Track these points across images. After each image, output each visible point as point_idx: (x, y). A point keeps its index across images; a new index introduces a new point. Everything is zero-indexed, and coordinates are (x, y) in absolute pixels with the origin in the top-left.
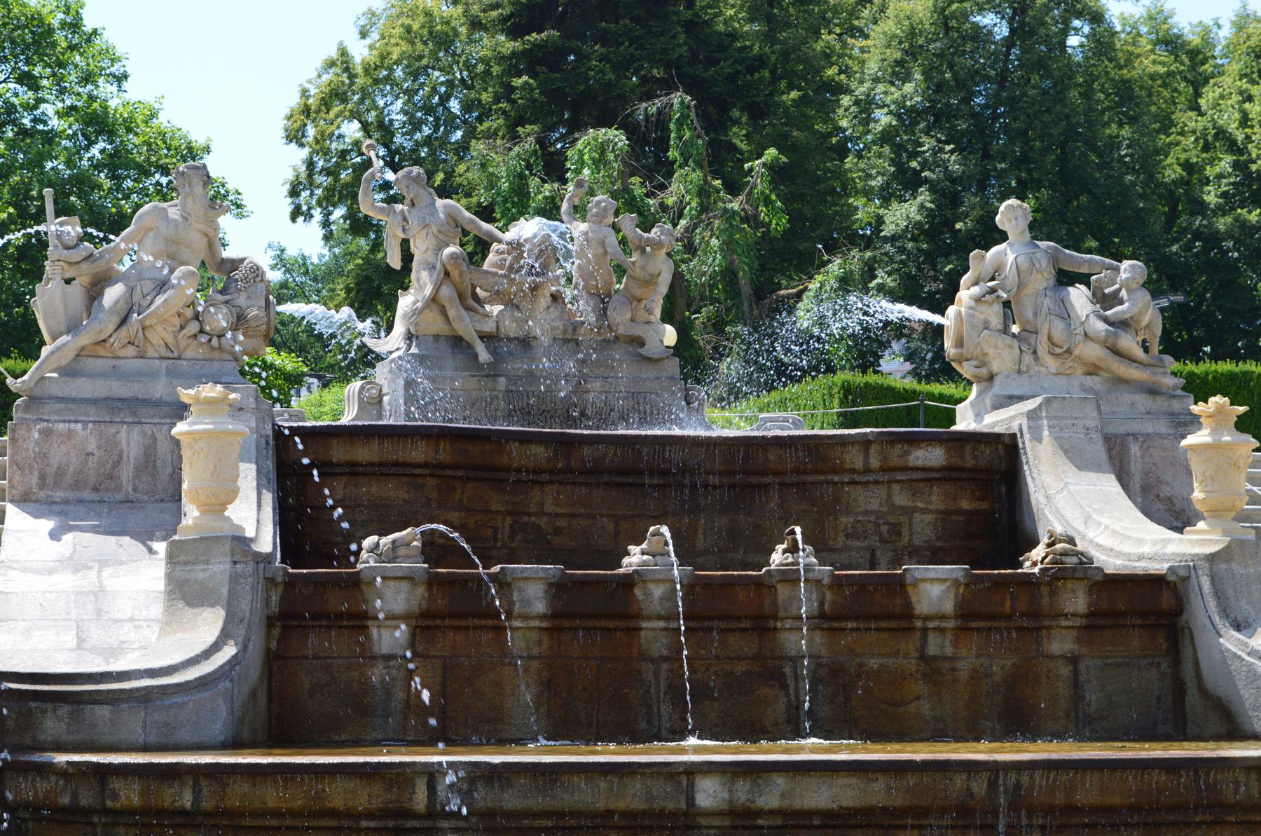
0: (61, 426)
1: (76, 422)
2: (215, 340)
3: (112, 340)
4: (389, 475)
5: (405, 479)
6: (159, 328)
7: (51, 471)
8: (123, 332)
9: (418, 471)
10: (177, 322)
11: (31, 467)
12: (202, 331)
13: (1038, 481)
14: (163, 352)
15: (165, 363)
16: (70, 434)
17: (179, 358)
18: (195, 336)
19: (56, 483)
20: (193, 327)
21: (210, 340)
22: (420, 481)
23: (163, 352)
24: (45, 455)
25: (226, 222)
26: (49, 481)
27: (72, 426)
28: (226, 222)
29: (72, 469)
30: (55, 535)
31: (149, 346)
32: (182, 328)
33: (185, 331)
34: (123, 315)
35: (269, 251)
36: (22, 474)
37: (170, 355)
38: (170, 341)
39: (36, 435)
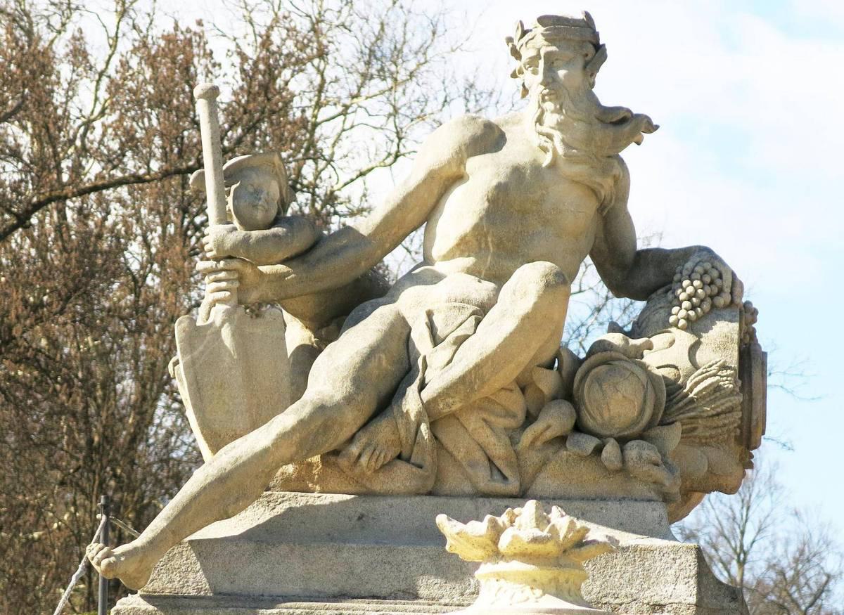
2: (610, 450)
3: (354, 450)
6: (473, 422)
8: (383, 430)
10: (517, 403)
13: (718, 360)
14: (483, 479)
18: (561, 440)
20: (555, 420)
21: (598, 451)
23: (483, 479)
25: (316, 189)
28: (316, 189)
30: (91, 55)
32: (530, 419)
33: (537, 427)
34: (384, 387)
35: (205, 233)
37: (499, 486)
38: (498, 449)
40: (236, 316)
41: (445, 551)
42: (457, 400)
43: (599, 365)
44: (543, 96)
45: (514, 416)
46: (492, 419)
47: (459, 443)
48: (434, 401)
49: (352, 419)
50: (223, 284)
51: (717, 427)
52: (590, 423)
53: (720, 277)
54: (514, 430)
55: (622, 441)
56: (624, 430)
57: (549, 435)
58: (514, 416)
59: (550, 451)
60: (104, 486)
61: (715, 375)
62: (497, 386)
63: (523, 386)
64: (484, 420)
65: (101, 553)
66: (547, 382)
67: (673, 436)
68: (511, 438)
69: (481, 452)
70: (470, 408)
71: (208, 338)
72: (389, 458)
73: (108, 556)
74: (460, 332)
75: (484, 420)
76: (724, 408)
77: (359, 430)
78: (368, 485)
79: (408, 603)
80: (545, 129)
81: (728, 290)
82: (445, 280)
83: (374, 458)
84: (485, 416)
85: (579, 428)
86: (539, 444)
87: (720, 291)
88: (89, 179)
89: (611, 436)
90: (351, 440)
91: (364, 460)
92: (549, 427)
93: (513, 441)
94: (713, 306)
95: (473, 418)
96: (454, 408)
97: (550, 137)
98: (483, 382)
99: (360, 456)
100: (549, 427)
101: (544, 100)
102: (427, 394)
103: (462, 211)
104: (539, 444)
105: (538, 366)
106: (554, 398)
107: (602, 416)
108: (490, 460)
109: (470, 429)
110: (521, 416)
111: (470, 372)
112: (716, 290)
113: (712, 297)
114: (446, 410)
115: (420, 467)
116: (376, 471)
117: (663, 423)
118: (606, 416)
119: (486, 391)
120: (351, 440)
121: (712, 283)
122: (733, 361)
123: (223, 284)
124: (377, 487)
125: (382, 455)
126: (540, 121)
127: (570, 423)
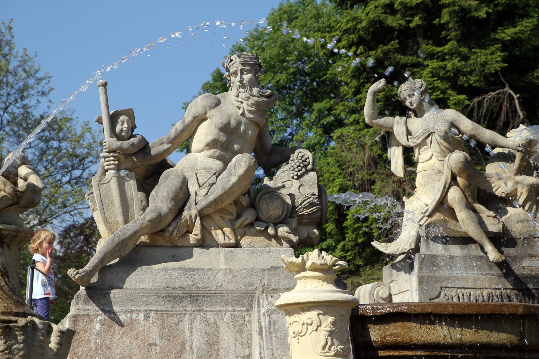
3: (171, 229)
18: (251, 225)
32: (239, 216)
42: (211, 208)
43: (264, 194)
44: (240, 86)
45: (233, 215)
46: (224, 216)
48: (203, 209)
50: (112, 162)
51: (311, 218)
52: (262, 217)
54: (232, 220)
56: (277, 219)
57: (247, 222)
58: (233, 215)
59: (247, 229)
60: (25, 94)
61: (310, 198)
62: (227, 203)
63: (236, 203)
65: (75, 273)
66: (245, 201)
68: (231, 224)
70: (216, 212)
73: (77, 273)
74: (211, 181)
77: (172, 221)
78: (175, 243)
80: (239, 99)
82: (514, 172)
84: (222, 215)
85: (258, 219)
89: (270, 222)
90: (169, 225)
91: (175, 233)
92: (247, 219)
94: (306, 170)
95: (217, 216)
96: (210, 212)
97: (242, 102)
98: (222, 201)
99: (173, 232)
100: (247, 219)
101: (240, 88)
102: (199, 207)
103: (204, 134)
104: (242, 226)
106: (248, 207)
107: (267, 214)
109: (215, 220)
110: (235, 215)
111: (217, 198)
114: (207, 213)
116: (179, 238)
117: (290, 217)
118: (269, 214)
119: (222, 206)
120: (169, 225)
122: (316, 192)
123: (112, 162)
124: (179, 244)
126: (237, 96)
127: (254, 217)
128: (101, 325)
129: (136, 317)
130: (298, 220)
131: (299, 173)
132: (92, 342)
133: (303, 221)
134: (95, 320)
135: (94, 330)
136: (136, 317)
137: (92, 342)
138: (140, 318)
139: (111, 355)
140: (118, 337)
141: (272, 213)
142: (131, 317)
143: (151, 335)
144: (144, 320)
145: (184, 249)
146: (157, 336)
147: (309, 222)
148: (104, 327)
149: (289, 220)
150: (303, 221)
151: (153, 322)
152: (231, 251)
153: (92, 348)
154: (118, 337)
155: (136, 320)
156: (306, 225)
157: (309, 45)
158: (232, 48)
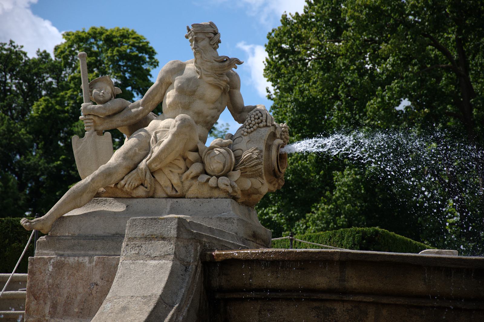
0: (71, 260)
1: (84, 256)
4: (246, 299)
5: (316, 304)
7: (61, 300)
9: (324, 296)
11: (45, 297)
12: (205, 172)
15: (170, 201)
16: (79, 266)
17: (183, 197)
18: (196, 177)
19: (65, 311)
20: (196, 168)
22: (328, 305)
23: (169, 191)
24: (58, 286)
26: (60, 309)
27: (81, 259)
29: (79, 298)
31: (158, 187)
33: (188, 172)
36: (38, 304)
39: (51, 268)
40: (93, 135)
41: (305, 214)
46: (173, 170)
47: (162, 179)
49: (122, 171)
51: (253, 171)
53: (262, 116)
55: (218, 177)
57: (192, 175)
64: (170, 171)
67: (236, 175)
69: (170, 182)
71: (83, 143)
72: (136, 185)
75: (170, 171)
76: (253, 164)
79: (211, 230)
81: (264, 121)
83: (130, 185)
84: (171, 169)
86: (189, 178)
87: (262, 121)
88: (123, 62)
93: (180, 177)
104: (189, 178)
105: (189, 151)
108: (173, 186)
112: (259, 120)
113: (258, 123)
115: (146, 188)
117: (234, 170)
121: (259, 118)
125: (133, 184)
128: (54, 267)
129: (82, 260)
130: (242, 173)
131: (249, 130)
132: (46, 282)
133: (248, 173)
134: (49, 263)
135: (47, 272)
136: (82, 260)
137: (46, 282)
138: (85, 261)
139: (60, 293)
140: (66, 278)
141: (214, 167)
142: (78, 260)
143: (93, 276)
144: (89, 263)
145: (138, 200)
146: (98, 277)
147: (252, 174)
148: (56, 268)
149: (232, 173)
150: (248, 173)
151: (96, 265)
152: (177, 202)
153: (45, 286)
154: (66, 278)
155: (81, 263)
156: (252, 177)
157: (279, 29)
158: (267, 79)
